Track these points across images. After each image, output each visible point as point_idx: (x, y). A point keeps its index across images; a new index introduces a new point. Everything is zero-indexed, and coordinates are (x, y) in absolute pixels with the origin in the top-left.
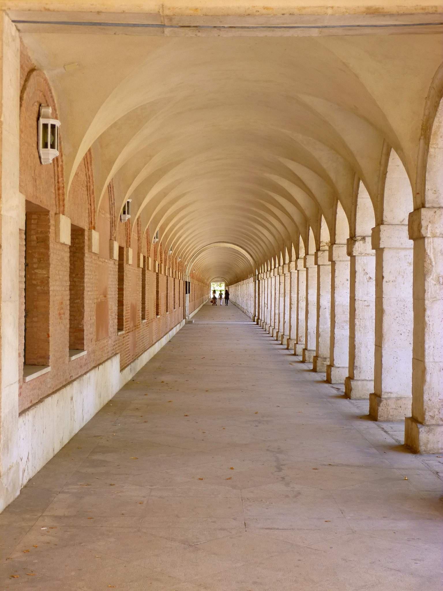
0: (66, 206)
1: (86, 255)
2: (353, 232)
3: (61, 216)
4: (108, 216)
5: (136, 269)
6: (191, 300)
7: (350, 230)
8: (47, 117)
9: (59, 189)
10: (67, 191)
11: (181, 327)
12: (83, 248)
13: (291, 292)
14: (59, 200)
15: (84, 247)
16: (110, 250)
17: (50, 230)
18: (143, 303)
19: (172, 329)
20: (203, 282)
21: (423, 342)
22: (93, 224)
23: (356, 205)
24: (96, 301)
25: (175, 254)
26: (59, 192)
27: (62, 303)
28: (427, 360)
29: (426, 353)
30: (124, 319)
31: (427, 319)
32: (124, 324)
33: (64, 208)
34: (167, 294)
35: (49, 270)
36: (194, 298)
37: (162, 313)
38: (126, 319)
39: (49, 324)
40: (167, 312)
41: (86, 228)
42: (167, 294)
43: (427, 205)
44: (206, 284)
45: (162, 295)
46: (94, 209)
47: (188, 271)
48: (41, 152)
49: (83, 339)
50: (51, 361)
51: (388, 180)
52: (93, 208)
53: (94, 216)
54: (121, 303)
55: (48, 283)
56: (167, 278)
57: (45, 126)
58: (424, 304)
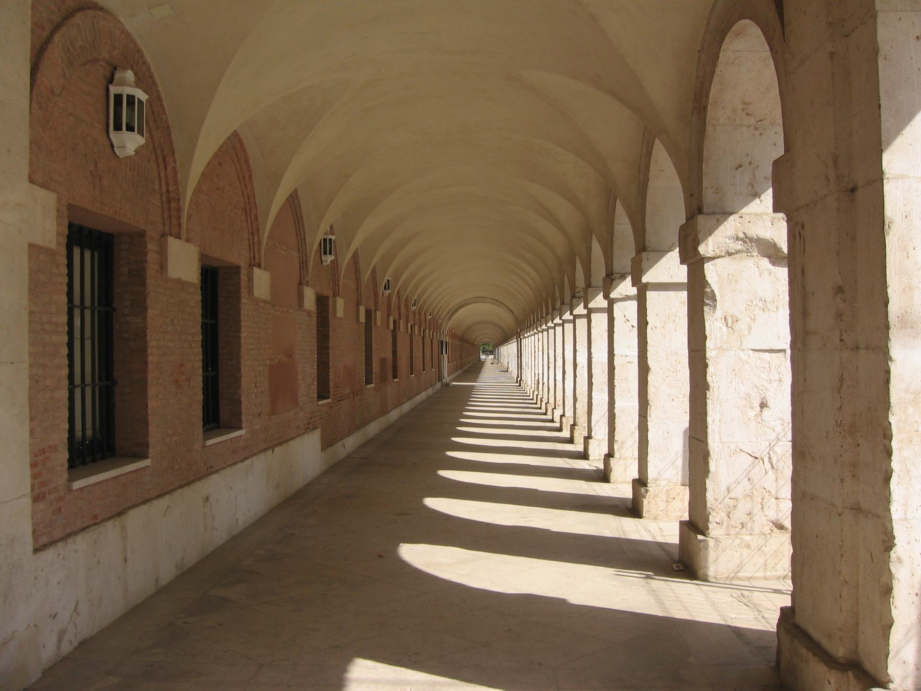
1: (244, 300)
3: (171, 240)
4: (295, 254)
7: (607, 266)
9: (169, 201)
12: (238, 291)
15: (239, 289)
17: (148, 259)
21: (704, 414)
23: (613, 233)
24: (268, 362)
27: (182, 365)
28: (710, 441)
29: (710, 431)
31: (709, 378)
41: (243, 264)
43: (705, 210)
46: (259, 240)
48: (112, 136)
49: (240, 414)
50: (151, 452)
51: (649, 191)
53: (259, 249)
55: (145, 336)
57: (118, 98)
58: (704, 357)
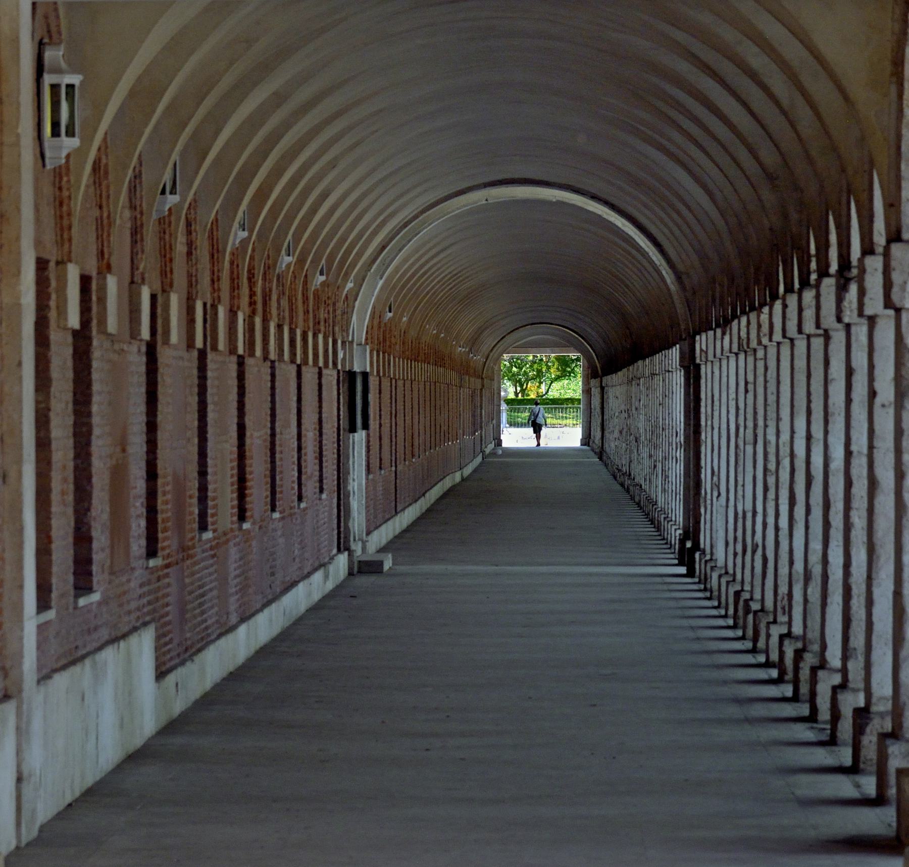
0: (74, 242)
1: (95, 343)
2: (867, 240)
5: (186, 355)
6: (375, 462)
8: (58, 71)
10: (76, 204)
11: (330, 585)
13: (826, 432)
14: (62, 229)
16: (131, 312)
18: (203, 473)
19: (294, 584)
20: (440, 359)
22: (106, 256)
25: (301, 261)
26: (61, 211)
30: (160, 520)
32: (160, 535)
33: (70, 245)
34: (273, 435)
35: (48, 393)
36: (394, 452)
37: (257, 516)
38: (163, 521)
39: (50, 512)
40: (273, 510)
41: (94, 274)
42: (273, 435)
44: (465, 369)
45: (257, 438)
46: (109, 217)
47: (359, 324)
48: (46, 145)
52: (105, 215)
53: (109, 235)
54: (152, 474)
56: (273, 367)
